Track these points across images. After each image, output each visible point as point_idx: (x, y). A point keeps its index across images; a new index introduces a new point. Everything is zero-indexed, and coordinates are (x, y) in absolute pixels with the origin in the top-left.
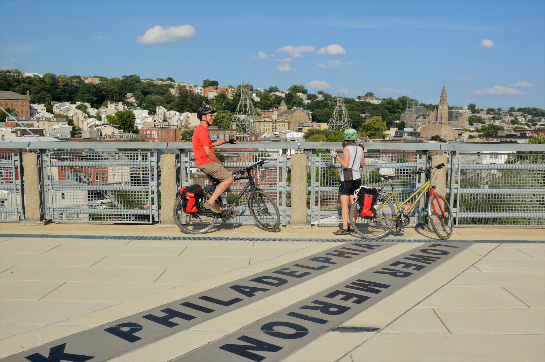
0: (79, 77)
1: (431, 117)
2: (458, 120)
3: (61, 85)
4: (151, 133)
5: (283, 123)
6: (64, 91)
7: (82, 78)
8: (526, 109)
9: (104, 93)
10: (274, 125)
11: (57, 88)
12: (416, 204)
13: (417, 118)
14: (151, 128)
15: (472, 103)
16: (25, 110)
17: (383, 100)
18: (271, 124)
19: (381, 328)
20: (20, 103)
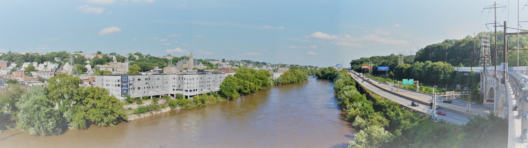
0: (37, 53)
1: (187, 64)
2: (198, 65)
3: (29, 56)
4: (501, 49)
5: (110, 68)
6: (31, 58)
7: (39, 54)
8: (245, 60)
9: (45, 58)
10: (106, 69)
11: (28, 58)
12: (517, 64)
13: (183, 64)
14: (235, 61)
15: (224, 58)
16: (5, 66)
17: (174, 57)
18: (105, 68)
19: (134, 90)
20: (4, 64)
